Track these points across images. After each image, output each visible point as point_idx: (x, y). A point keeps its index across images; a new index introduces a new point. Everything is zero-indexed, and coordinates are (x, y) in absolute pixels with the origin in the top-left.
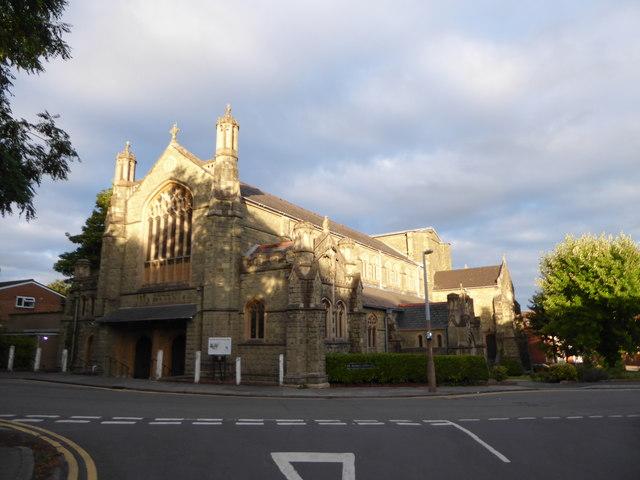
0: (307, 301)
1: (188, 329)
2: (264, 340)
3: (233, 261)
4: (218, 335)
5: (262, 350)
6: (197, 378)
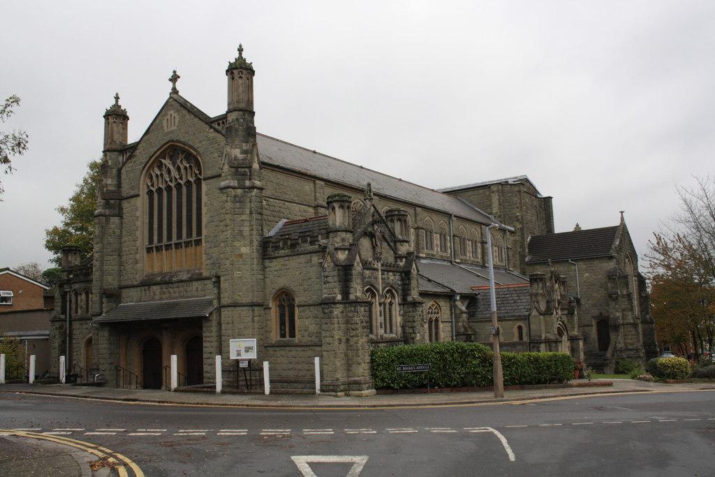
0: (346, 292)
1: (204, 329)
2: (296, 340)
3: (255, 243)
4: (241, 335)
5: (295, 352)
6: (219, 388)
